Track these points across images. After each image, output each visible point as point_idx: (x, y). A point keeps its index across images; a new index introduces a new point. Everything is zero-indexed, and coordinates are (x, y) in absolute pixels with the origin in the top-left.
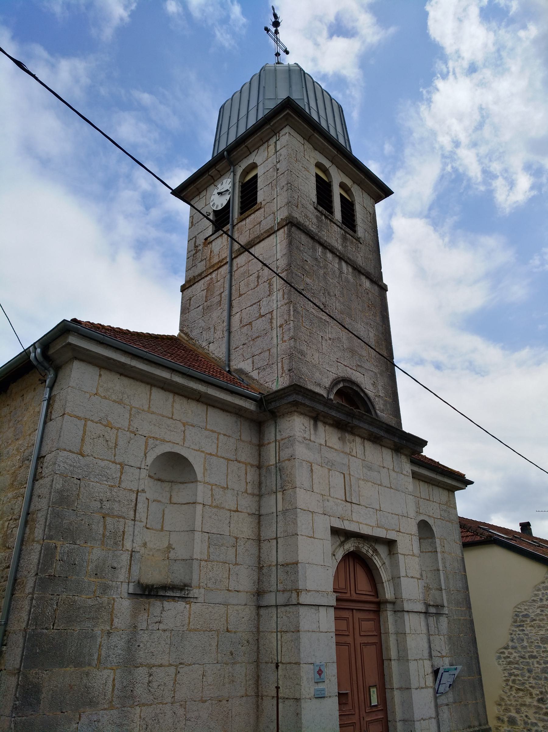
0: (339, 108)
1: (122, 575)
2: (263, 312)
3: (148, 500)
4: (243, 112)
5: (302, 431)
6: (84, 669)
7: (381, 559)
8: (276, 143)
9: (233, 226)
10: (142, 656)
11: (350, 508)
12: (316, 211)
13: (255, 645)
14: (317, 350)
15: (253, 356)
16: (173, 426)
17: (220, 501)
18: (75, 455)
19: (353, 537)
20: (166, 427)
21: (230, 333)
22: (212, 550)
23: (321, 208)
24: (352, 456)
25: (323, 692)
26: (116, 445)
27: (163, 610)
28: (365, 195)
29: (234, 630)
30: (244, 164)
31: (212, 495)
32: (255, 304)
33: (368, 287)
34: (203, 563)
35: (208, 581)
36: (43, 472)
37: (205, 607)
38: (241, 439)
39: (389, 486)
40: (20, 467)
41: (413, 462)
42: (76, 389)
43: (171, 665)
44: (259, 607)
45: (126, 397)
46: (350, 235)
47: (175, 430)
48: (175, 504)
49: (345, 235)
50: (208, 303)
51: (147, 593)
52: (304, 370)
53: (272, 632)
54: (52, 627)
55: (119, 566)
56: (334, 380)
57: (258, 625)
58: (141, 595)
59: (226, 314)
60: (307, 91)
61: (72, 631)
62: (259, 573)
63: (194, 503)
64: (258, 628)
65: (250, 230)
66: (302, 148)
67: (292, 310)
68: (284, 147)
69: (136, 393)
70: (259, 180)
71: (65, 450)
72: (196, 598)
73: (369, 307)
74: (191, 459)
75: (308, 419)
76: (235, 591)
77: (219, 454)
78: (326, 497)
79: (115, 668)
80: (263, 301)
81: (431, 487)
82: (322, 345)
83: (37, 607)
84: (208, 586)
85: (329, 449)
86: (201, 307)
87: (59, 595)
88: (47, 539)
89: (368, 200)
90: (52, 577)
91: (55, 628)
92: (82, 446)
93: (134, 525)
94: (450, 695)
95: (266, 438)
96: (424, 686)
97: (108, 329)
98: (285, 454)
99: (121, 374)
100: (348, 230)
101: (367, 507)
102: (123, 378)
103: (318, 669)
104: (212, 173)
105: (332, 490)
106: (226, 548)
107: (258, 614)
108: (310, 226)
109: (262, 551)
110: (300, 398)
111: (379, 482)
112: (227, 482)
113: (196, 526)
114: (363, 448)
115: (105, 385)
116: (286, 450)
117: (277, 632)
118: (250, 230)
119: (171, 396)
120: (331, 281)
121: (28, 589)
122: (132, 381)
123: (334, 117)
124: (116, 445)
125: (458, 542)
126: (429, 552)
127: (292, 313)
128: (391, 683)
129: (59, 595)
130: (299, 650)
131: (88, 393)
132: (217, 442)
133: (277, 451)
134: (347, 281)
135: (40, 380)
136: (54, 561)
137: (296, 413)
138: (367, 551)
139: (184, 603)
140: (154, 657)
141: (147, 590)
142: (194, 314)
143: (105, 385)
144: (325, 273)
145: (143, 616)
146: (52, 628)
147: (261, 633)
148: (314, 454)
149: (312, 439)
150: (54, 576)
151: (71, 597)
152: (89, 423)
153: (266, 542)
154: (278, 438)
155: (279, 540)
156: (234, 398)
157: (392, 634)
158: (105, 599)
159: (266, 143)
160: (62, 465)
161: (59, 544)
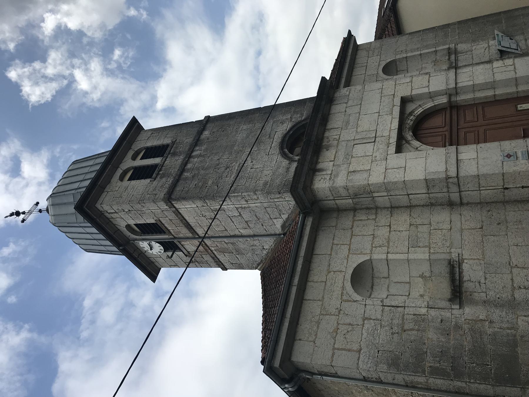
0: (75, 163)
1: (447, 314)
2: (237, 214)
3: (388, 295)
4: (88, 236)
5: (325, 181)
6: (518, 340)
8: (109, 213)
9: (175, 238)
10: (506, 295)
11: (380, 138)
12: (157, 179)
13: (490, 204)
14: (262, 172)
15: (271, 218)
16: (331, 281)
17: (384, 240)
18: (361, 356)
19: (402, 133)
20: (332, 286)
21: (254, 236)
22: (421, 244)
23: (154, 175)
24: (339, 139)
25: (524, 153)
26: (350, 324)
27: (470, 281)
28: (139, 138)
29: (481, 223)
30: (128, 234)
31: (380, 246)
32: (232, 220)
33: (209, 132)
34: (432, 251)
35: (445, 246)
36: (375, 377)
37: (465, 247)
38: (335, 226)
39: (359, 106)
40: (373, 391)
41: (337, 87)
42: (312, 358)
43: (511, 272)
44: (462, 204)
45: (314, 319)
46: (171, 150)
47: (334, 279)
48: (389, 275)
49: (172, 154)
50: (234, 251)
51: (458, 294)
52: (278, 181)
53: (480, 193)
54: (490, 366)
55: (440, 317)
56: (283, 157)
57: (475, 203)
58: (460, 298)
59: (241, 239)
60: (67, 191)
61: (491, 350)
62: (436, 205)
63: (387, 260)
64: (478, 203)
65: (176, 226)
66: (111, 193)
67: (234, 195)
68: (111, 207)
69: (310, 311)
70: (139, 223)
71: (358, 364)
72: (458, 254)
73: (223, 131)
74: (355, 265)
75: (315, 177)
76: (451, 224)
77: (348, 243)
78: (373, 159)
79: (516, 316)
80: (229, 215)
81: (356, 66)
82: (257, 168)
83: (476, 378)
84: (449, 246)
85: (336, 158)
86: (237, 256)
87: (466, 362)
88: (425, 374)
89: (142, 136)
90: (453, 368)
91: (490, 364)
92: (354, 351)
93: (408, 307)
94: (517, 38)
95: (333, 206)
96: (513, 67)
97: (264, 333)
98: (343, 193)
99: (297, 324)
100: (167, 152)
101: (378, 124)
102: (300, 323)
103: (506, 158)
104: (137, 256)
105: (367, 154)
106: (419, 233)
107: (468, 204)
108: (169, 183)
109: (418, 204)
110: (301, 186)
111: (358, 115)
112: (369, 235)
113: (404, 258)
114: (332, 130)
115: (307, 335)
116: (340, 192)
117: (480, 190)
118: (176, 226)
119: (309, 284)
120: (208, 164)
121: (464, 385)
122: (301, 315)
123: (82, 167)
124: (350, 324)
125: (397, 39)
126: (407, 63)
127: (236, 194)
128: (513, 93)
129: (466, 362)
130: (493, 174)
131: (314, 349)
132: (339, 245)
133: (342, 198)
134: (206, 150)
135: (308, 382)
136: (441, 368)
137: (312, 187)
138: (411, 120)
139: (464, 264)
140: (506, 286)
141: (456, 294)
142: (242, 261)
143: (307, 335)
144: (203, 169)
145: (476, 296)
146: (490, 366)
147: (482, 201)
148: (341, 170)
149: (330, 172)
150: (452, 367)
151: (466, 353)
152: (336, 346)
153: (411, 202)
154: (332, 198)
155: (409, 193)
156: (305, 235)
157: (474, 96)
158: (466, 327)
159: (110, 219)
160: (369, 365)
161: (428, 365)
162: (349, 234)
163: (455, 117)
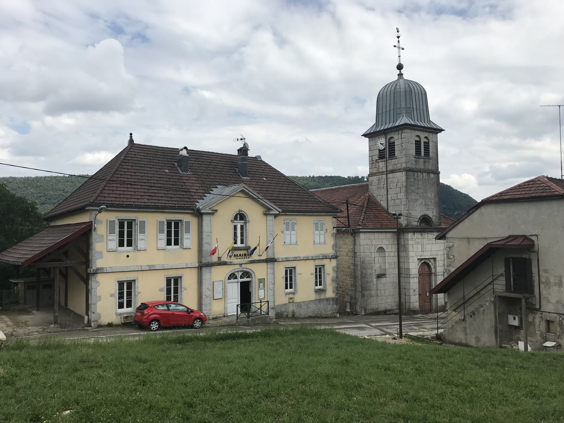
7: (431, 262)
98: (406, 243)
162: (392, 244)
163: (427, 274)
